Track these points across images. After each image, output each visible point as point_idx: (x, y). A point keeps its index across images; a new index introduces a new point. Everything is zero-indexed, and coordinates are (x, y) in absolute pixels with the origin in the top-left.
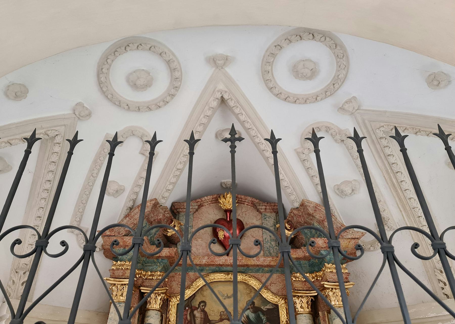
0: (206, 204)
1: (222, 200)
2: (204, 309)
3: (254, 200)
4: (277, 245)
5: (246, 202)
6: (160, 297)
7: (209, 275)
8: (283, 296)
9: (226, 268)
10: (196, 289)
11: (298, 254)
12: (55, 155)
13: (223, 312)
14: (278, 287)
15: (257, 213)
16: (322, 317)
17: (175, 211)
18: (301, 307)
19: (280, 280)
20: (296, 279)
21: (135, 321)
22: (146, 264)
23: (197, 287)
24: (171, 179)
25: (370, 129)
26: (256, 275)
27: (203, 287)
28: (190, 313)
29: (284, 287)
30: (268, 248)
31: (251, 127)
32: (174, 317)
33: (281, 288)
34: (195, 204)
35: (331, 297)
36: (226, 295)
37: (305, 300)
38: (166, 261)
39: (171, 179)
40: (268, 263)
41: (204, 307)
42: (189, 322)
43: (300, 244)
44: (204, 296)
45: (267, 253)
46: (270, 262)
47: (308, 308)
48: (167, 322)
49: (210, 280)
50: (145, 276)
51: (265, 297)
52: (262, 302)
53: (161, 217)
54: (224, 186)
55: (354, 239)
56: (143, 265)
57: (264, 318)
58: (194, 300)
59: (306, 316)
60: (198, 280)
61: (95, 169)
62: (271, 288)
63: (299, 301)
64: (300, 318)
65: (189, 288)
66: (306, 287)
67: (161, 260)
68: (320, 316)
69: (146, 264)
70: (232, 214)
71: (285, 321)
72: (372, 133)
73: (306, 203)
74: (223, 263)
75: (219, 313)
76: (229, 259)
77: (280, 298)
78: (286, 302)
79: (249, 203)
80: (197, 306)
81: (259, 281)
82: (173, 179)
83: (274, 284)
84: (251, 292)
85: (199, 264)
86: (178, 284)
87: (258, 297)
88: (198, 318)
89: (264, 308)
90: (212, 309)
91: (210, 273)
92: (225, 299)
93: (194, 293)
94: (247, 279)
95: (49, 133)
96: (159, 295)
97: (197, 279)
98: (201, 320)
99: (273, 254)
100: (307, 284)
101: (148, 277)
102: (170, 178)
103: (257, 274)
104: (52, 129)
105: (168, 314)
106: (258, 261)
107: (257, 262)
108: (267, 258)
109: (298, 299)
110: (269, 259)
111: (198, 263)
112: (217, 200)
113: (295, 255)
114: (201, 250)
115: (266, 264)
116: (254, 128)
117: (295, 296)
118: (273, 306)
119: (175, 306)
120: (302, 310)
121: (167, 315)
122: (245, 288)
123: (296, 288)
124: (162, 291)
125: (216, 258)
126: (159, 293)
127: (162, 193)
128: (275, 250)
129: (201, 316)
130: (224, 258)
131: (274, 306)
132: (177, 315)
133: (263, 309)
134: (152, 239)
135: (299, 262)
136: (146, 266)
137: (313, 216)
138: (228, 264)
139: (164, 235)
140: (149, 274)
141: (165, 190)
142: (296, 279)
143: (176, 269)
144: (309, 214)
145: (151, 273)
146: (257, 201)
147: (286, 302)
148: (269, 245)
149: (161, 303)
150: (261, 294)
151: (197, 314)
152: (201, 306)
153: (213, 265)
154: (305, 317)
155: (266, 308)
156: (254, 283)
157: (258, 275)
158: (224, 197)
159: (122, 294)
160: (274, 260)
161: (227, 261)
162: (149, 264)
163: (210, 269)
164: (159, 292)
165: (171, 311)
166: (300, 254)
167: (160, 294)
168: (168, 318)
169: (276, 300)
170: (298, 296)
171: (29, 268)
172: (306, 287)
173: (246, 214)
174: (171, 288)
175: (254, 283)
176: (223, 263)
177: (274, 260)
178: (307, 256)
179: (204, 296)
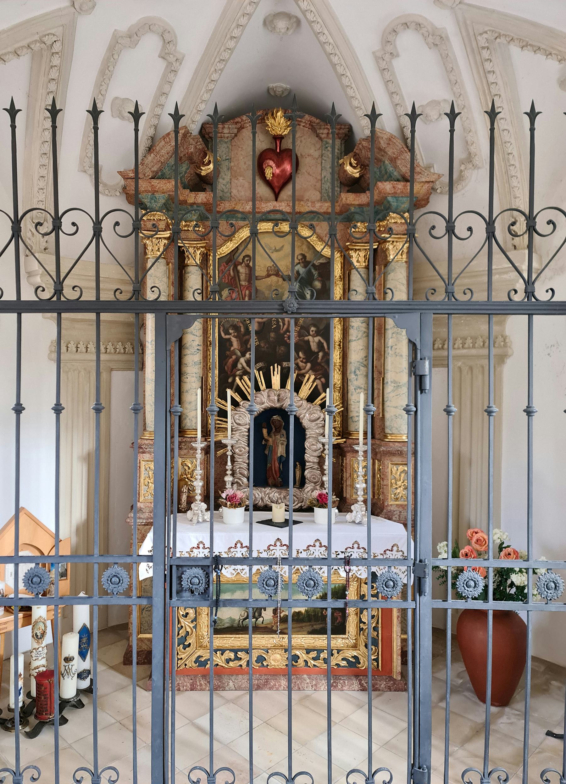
0: (248, 125)
1: (270, 122)
3: (314, 119)
5: (302, 122)
6: (200, 252)
12: (55, 70)
15: (317, 139)
17: (207, 136)
18: (358, 261)
23: (241, 239)
24: (203, 94)
25: (471, 33)
28: (234, 268)
30: (326, 190)
31: (315, 19)
34: (234, 126)
36: (274, 248)
37: (362, 254)
38: (202, 208)
39: (203, 94)
42: (232, 278)
43: (366, 184)
53: (192, 150)
54: (272, 93)
55: (428, 182)
60: (241, 231)
61: (103, 83)
65: (231, 241)
70: (283, 141)
71: (338, 276)
72: (473, 39)
73: (379, 134)
78: (341, 256)
79: (306, 124)
80: (241, 261)
82: (205, 95)
92: (272, 253)
95: (45, 39)
96: (198, 249)
102: (201, 94)
104: (48, 32)
112: (264, 119)
114: (243, 193)
116: (319, 20)
117: (352, 249)
120: (358, 264)
124: (202, 245)
127: (192, 114)
134: (183, 179)
137: (385, 152)
139: (196, 173)
140: (184, 224)
141: (195, 111)
143: (394, 317)
144: (380, 149)
146: (318, 121)
151: (242, 269)
152: (245, 260)
158: (273, 115)
159: (159, 249)
164: (198, 245)
170: (356, 249)
173: (301, 141)
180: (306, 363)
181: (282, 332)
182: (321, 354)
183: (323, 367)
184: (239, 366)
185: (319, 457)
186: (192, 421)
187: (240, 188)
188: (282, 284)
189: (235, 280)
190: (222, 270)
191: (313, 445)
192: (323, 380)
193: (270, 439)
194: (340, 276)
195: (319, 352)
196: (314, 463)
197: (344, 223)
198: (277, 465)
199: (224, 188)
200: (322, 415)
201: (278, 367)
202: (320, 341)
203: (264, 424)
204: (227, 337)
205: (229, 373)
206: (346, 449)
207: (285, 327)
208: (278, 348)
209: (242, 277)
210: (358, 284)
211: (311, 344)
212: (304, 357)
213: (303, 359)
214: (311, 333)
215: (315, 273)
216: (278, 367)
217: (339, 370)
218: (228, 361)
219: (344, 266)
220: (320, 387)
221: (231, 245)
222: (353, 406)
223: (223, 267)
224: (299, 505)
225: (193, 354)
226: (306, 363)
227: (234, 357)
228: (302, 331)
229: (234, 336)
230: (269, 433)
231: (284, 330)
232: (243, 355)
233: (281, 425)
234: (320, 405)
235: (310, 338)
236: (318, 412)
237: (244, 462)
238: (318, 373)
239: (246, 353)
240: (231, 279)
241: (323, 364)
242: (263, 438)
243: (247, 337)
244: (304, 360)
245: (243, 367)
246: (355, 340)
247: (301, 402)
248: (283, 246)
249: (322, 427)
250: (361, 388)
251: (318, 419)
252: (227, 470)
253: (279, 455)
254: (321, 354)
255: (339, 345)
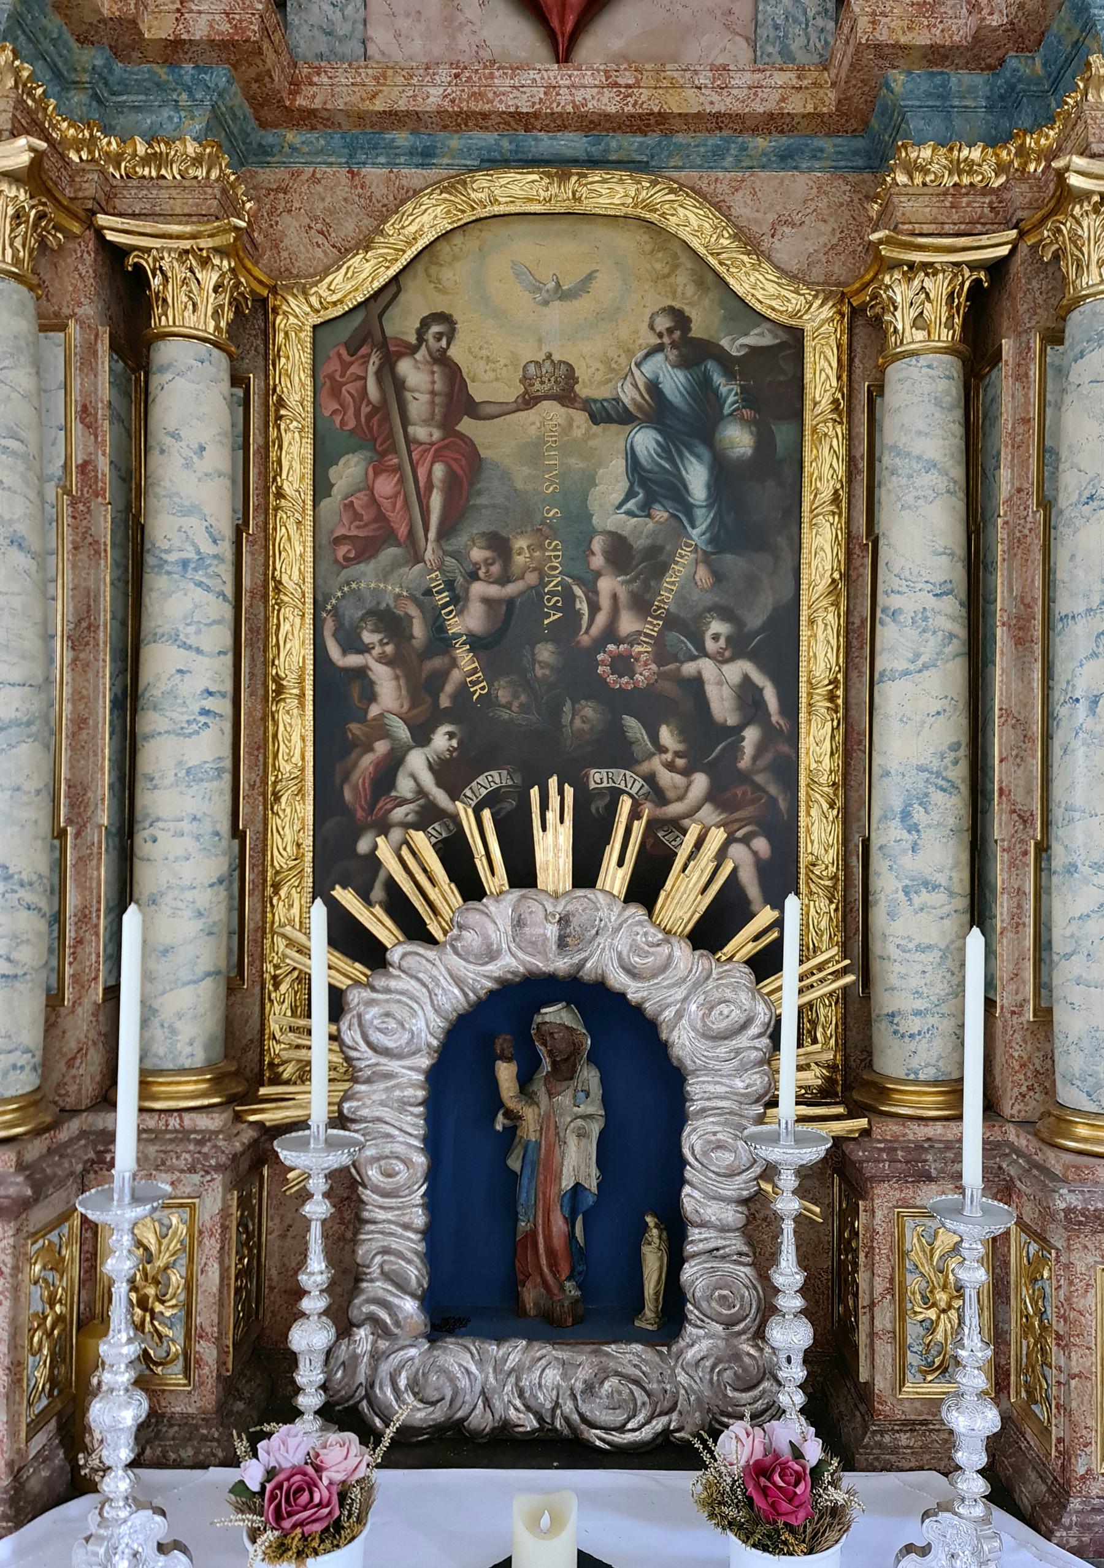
2: (445, 351)
4: (826, 11)
7: (464, 183)
8: (829, 285)
9: (550, 138)
10: (404, 252)
11: (941, 26)
13: (537, 363)
14: (808, 244)
16: (1010, 362)
18: (919, 322)
19: (822, 205)
20: (911, 178)
21: (95, 384)
22: (114, 98)
26: (703, 179)
27: (438, 246)
29: (841, 239)
30: (776, 27)
32: (303, 385)
33: (825, 245)
35: (1085, 249)
36: (551, 285)
37: (938, 286)
40: (771, 106)
41: (444, 343)
42: (376, 410)
44: (443, 291)
45: (769, 55)
46: (783, 99)
47: (949, 325)
48: (272, 409)
49: (473, 209)
50: (117, 162)
51: (740, 291)
52: (724, 318)
56: (95, 97)
57: (731, 390)
58: (395, 311)
59: (935, 364)
62: (777, 245)
63: (911, 294)
64: (901, 375)
65: (367, 249)
66: (955, 217)
67: (191, 72)
68: (1004, 357)
69: (114, 94)
71: (825, 404)
74: (534, 103)
75: (516, 371)
76: (568, 82)
77: (816, 297)
80: (412, 339)
81: (719, 210)
83: (793, 225)
84: (675, 267)
85: (408, 114)
86: (310, 228)
87: (710, 294)
88: (416, 395)
89: (734, 346)
90: (484, 352)
91: (471, 171)
92: (546, 303)
93: (391, 272)
94: (658, 198)
97: (403, 202)
98: (432, 403)
99: (801, 57)
100: (965, 200)
101: (134, 167)
103: (713, 175)
105: (271, 372)
106: (720, 94)
107: (715, 98)
108: (768, 73)
109: (910, 280)
110: (779, 78)
111: (402, 105)
113: (926, 31)
115: (761, 110)
118: (776, 336)
119: (302, 335)
120: (920, 335)
121: (267, 376)
122: (648, 248)
123: (903, 223)
125: (497, 74)
126: (201, 250)
128: (814, 36)
129: (433, 382)
130: (542, 78)
131: (780, 332)
132: (314, 376)
133: (727, 347)
135: (938, 80)
136: (120, 108)
138: (559, 109)
140: (141, 149)
142: (911, 178)
145: (151, 146)
147: (843, 316)
148: (786, 11)
149: (222, 306)
150: (723, 280)
153: (485, 116)
154: (929, 367)
155: (742, 346)
156: (692, 218)
157: (716, 180)
160: (805, 83)
161: (558, 94)
162: (132, 98)
163: (469, 149)
165: (283, 360)
166: (954, 28)
167: (208, 257)
168: (274, 390)
169: (796, 302)
170: (911, 266)
171: (302, 669)
172: (955, 217)
174: (277, 246)
175: (692, 218)
176: (534, 103)
177: (805, 83)
178: (996, 29)
179: (443, 291)
180: (687, 772)
181: (585, 640)
182: (751, 736)
183: (758, 788)
184: (404, 786)
185: (745, 1202)
186: (173, 1031)
187: (403, 24)
188: (587, 437)
189: (387, 418)
190: (331, 377)
191: (720, 1146)
192: (761, 845)
193: (530, 1115)
194: (835, 402)
195: (742, 727)
196: (723, 1229)
197: (852, 177)
198: (559, 1225)
199: (337, 16)
200: (761, 1008)
201: (561, 792)
202: (746, 678)
203: (503, 1043)
204: (354, 660)
205: (360, 814)
206: (869, 1169)
207: (601, 619)
208: (567, 708)
209: (418, 406)
210: (921, 425)
211: (712, 691)
212: (679, 747)
213: (677, 754)
214: (710, 646)
215: (729, 391)
216: (561, 792)
217: (832, 806)
218: (355, 765)
219: (851, 360)
220: (749, 880)
221: (368, 267)
222: (897, 968)
223: (334, 366)
224: (658, 1424)
225: (180, 733)
226: (687, 772)
227: (382, 747)
228: (674, 636)
229: (383, 659)
230: (524, 1081)
231: (595, 630)
232: (422, 738)
233: (575, 1051)
234: (751, 962)
235: (706, 668)
236: (744, 997)
237: (406, 1227)
238: (738, 815)
239: (433, 730)
240: (369, 417)
241: (759, 779)
242: (499, 1103)
243: (437, 662)
244: (680, 762)
245: (421, 792)
246: (906, 673)
247: (665, 950)
248: (590, 277)
249: (761, 1063)
250: (936, 887)
251: (745, 1026)
252: (301, 1293)
253: (567, 1183)
254: (751, 736)
255: (832, 698)
